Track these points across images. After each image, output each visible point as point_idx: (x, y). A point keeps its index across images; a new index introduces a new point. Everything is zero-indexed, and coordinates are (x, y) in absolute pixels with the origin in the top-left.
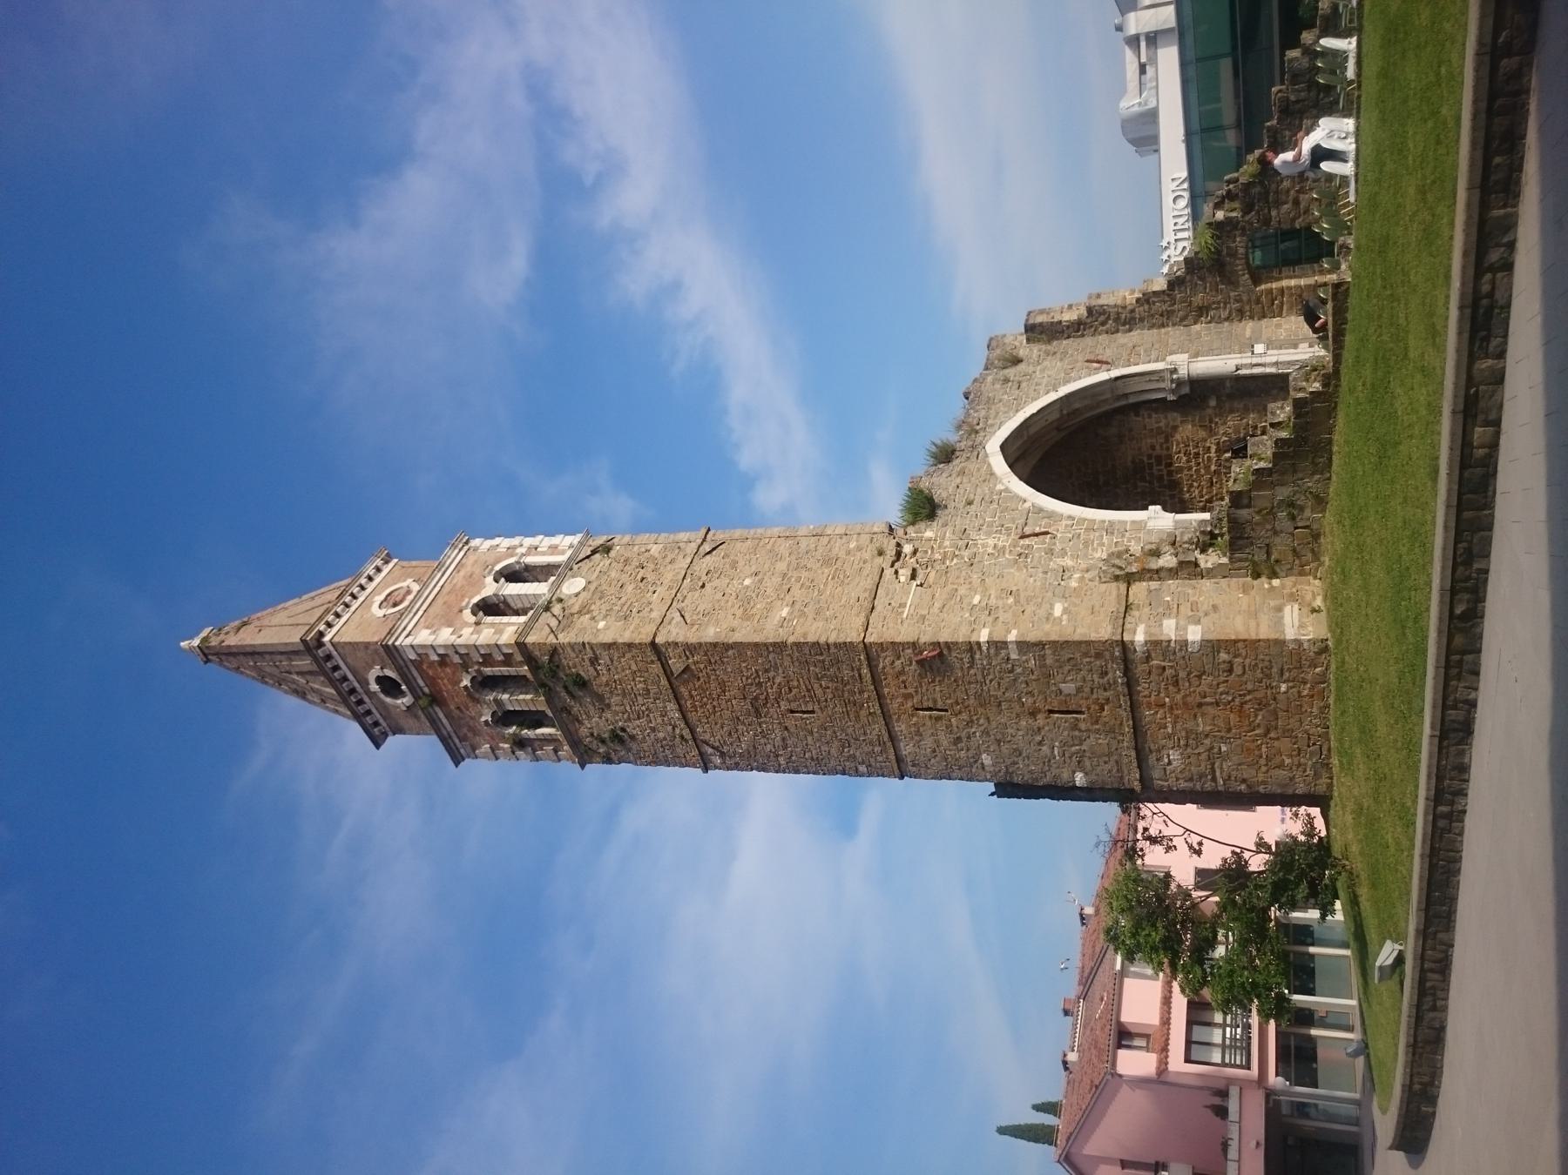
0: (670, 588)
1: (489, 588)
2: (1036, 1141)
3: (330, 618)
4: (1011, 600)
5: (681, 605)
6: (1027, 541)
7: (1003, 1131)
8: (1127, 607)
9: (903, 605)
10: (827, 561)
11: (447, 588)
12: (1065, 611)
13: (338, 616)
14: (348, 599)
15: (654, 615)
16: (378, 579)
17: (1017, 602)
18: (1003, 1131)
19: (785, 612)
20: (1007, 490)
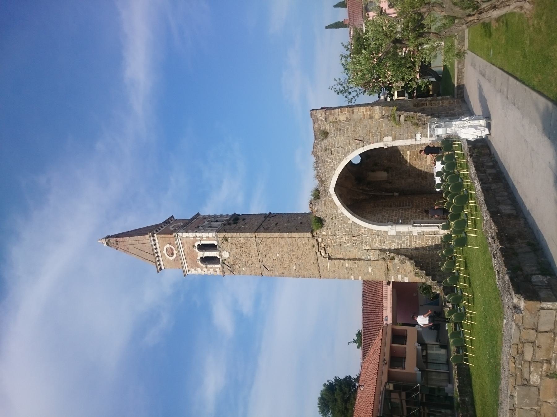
0: (256, 256)
1: (201, 254)
2: (339, 28)
3: (158, 263)
4: (356, 266)
5: (263, 264)
6: (354, 238)
7: (327, 27)
8: (388, 270)
9: (327, 266)
10: (299, 248)
11: (186, 253)
12: (372, 270)
13: (159, 261)
14: (156, 255)
15: (257, 266)
16: (158, 246)
17: (358, 266)
18: (327, 27)
19: (294, 267)
20: (342, 213)
